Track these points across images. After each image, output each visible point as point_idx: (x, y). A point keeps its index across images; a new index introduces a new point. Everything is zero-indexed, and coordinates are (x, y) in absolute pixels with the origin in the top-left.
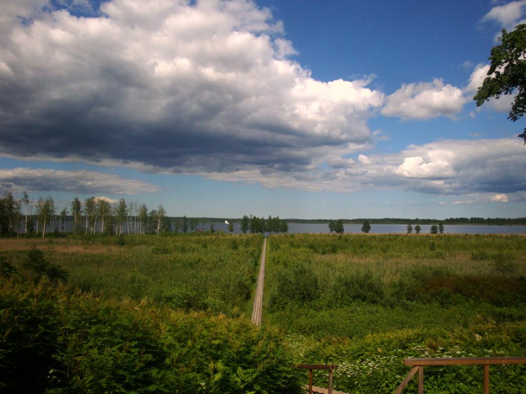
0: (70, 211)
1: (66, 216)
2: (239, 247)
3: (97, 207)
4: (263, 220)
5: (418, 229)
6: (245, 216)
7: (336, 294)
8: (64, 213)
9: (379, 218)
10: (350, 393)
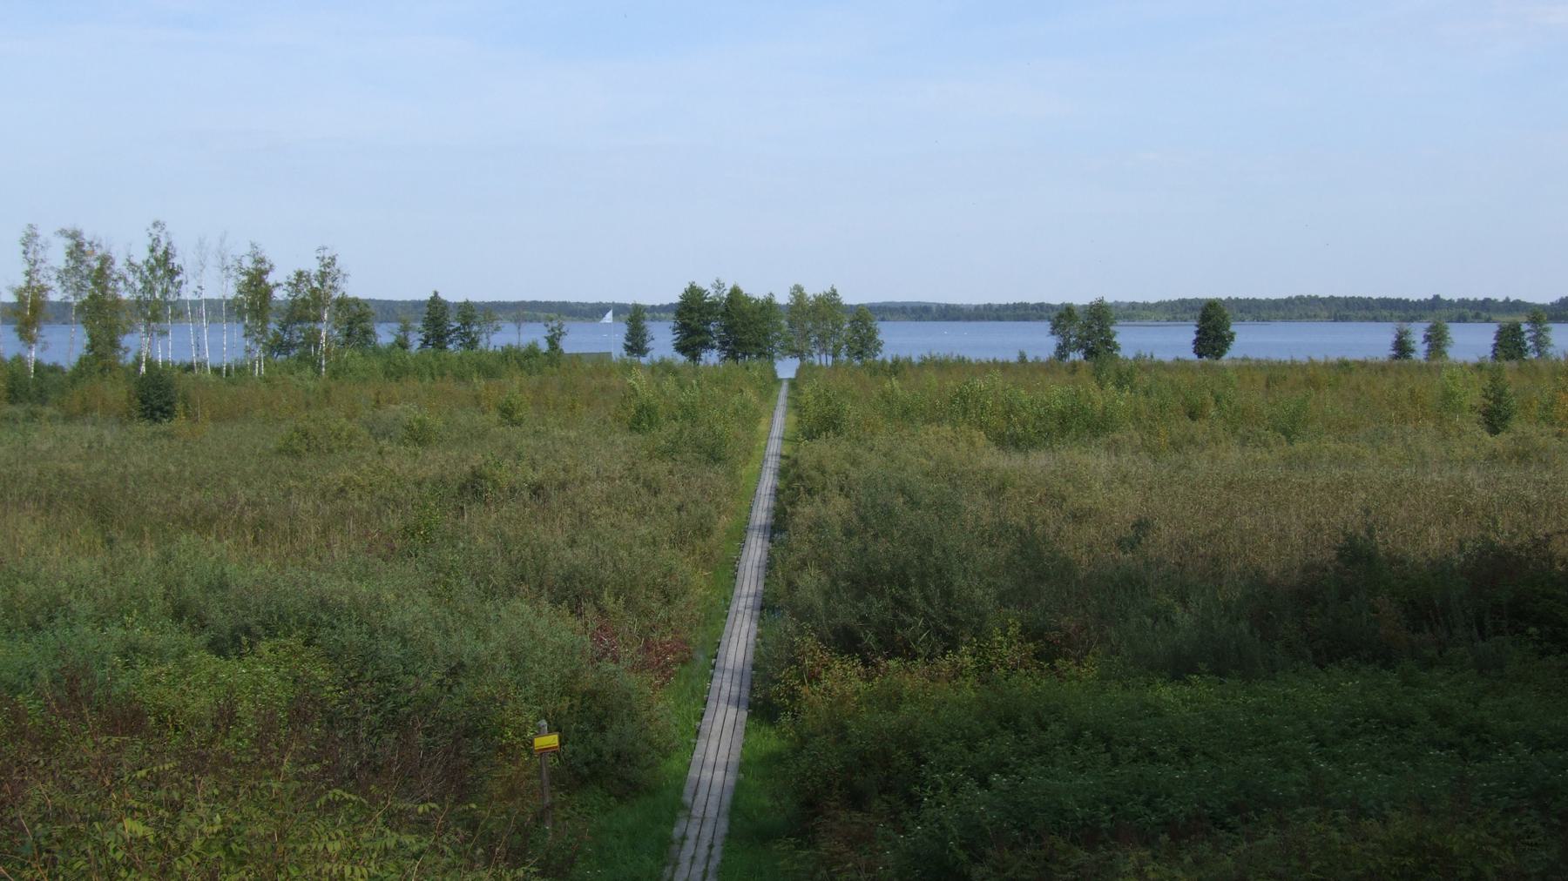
4: (768, 306)
5: (1436, 340)
6: (692, 287)
7: (595, 604)
9: (1242, 296)
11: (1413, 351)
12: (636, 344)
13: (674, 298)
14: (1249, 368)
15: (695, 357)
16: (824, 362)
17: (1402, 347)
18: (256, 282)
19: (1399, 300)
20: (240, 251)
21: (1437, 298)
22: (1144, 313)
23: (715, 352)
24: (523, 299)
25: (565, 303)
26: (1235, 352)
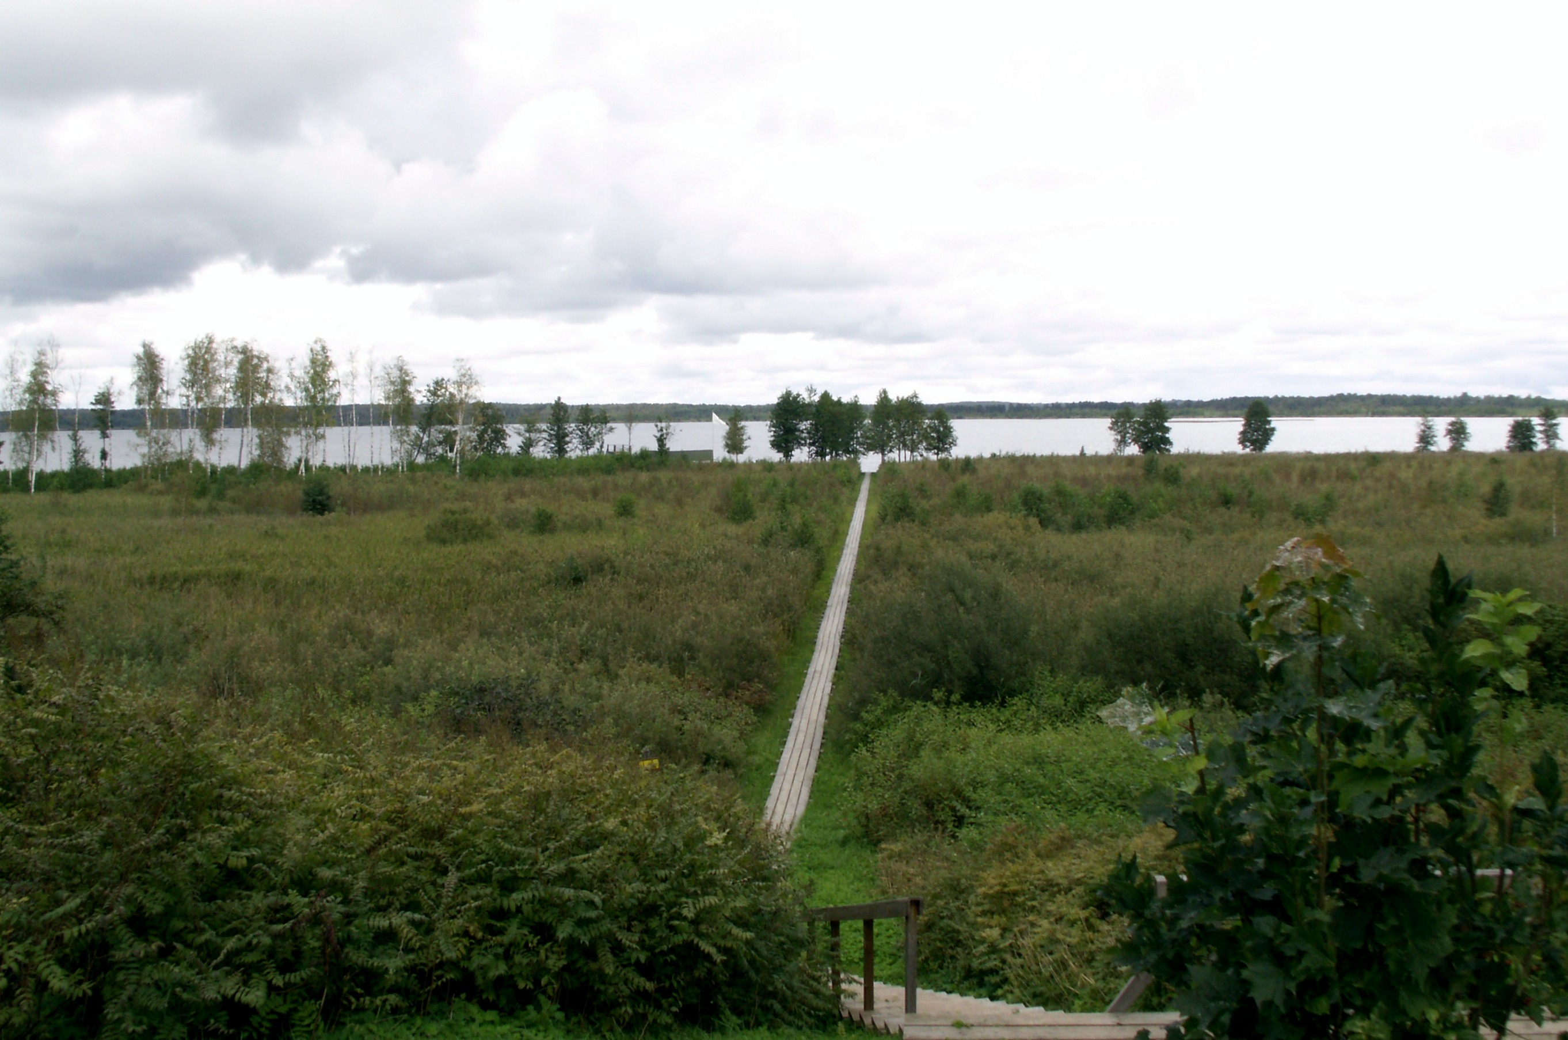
0: (126, 389)
1: (113, 413)
2: (758, 514)
3: (544, 426)
5: (1458, 432)
6: (788, 394)
8: (104, 399)
10: (808, 1037)
11: (1434, 436)
12: (735, 444)
13: (772, 399)
14: (1285, 462)
15: (788, 454)
16: (903, 460)
17: (1425, 438)
18: (402, 385)
19: (1431, 398)
20: (387, 357)
21: (1465, 395)
22: (1200, 410)
23: (806, 449)
24: (1200, 399)
25: (1234, 399)
26: (1273, 447)
